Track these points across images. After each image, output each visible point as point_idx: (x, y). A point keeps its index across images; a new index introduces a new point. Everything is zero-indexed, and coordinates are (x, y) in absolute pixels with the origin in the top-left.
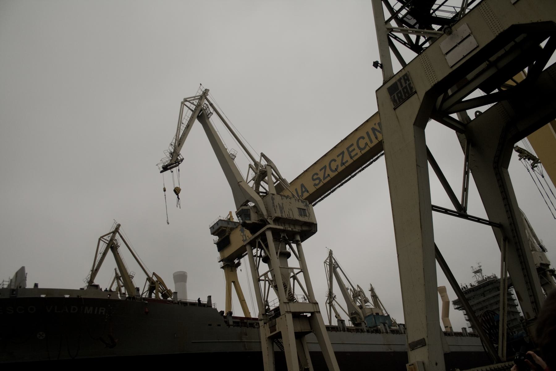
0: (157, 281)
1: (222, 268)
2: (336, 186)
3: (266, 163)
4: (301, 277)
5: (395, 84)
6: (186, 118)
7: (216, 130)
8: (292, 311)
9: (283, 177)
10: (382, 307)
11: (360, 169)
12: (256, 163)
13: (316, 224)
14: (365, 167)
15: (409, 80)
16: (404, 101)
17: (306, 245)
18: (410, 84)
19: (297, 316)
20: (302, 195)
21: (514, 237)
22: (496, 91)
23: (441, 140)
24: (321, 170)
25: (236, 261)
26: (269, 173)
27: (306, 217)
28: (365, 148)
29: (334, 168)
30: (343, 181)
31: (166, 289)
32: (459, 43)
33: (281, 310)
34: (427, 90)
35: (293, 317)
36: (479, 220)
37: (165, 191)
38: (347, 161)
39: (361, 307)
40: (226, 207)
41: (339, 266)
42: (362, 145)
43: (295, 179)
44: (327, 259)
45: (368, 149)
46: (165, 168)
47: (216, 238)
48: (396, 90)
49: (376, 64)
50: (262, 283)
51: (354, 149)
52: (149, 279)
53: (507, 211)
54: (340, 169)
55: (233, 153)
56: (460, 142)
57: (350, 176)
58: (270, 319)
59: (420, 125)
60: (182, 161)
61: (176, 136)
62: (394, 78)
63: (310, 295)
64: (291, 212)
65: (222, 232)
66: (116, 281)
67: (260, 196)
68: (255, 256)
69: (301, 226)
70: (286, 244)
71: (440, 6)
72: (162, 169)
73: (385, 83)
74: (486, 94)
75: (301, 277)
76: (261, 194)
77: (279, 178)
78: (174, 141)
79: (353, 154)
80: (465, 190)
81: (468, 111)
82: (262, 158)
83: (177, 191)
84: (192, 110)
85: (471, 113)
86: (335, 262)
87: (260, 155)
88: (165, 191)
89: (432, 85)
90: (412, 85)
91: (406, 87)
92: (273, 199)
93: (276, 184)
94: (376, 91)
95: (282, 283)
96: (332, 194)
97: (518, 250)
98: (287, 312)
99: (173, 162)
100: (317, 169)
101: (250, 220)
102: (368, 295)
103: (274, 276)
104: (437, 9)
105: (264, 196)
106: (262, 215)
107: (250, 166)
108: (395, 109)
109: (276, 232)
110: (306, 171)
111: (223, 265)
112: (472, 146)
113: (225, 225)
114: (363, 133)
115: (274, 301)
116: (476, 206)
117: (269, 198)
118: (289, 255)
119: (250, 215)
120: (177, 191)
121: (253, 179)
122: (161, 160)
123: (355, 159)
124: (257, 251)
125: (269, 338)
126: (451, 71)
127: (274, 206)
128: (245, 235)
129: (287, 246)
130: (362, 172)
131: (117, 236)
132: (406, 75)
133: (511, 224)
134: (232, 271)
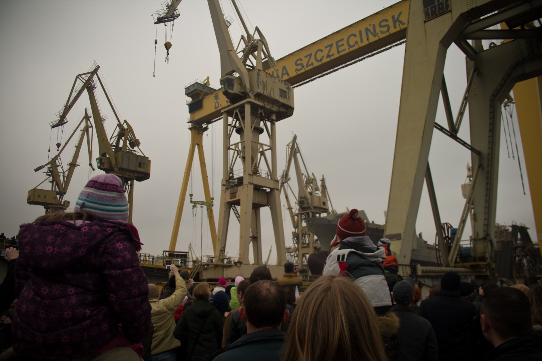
0: (127, 129)
1: (190, 129)
2: (317, 76)
3: (259, 38)
4: (268, 154)
8: (255, 183)
9: (272, 55)
10: (328, 198)
11: (344, 65)
12: (249, 35)
13: (293, 108)
14: (349, 65)
16: (437, 16)
17: (279, 124)
19: (258, 189)
20: (282, 77)
21: (488, 166)
22: (519, 28)
23: (456, 62)
24: (306, 57)
25: (204, 126)
26: (259, 49)
27: (285, 100)
28: (354, 46)
29: (319, 58)
30: (324, 73)
36: (464, 144)
37: (156, 43)
38: (333, 55)
39: (311, 194)
41: (299, 152)
42: (352, 42)
44: (290, 143)
45: (356, 47)
46: (160, 20)
47: (190, 100)
50: (231, 152)
51: (343, 45)
52: (120, 125)
54: (325, 60)
55: (229, 20)
56: (467, 68)
57: (332, 70)
58: (232, 187)
59: (445, 44)
60: (178, 17)
63: (272, 173)
64: (272, 91)
65: (197, 94)
66: (84, 121)
67: (247, 69)
68: (230, 125)
69: (279, 107)
72: (156, 21)
75: (268, 154)
76: (247, 67)
77: (269, 56)
80: (461, 114)
82: (256, 32)
83: (168, 46)
85: (486, 44)
86: (298, 147)
87: (255, 29)
88: (156, 43)
89: (470, 8)
90: (449, 3)
91: (442, 3)
92: (258, 75)
95: (251, 155)
96: (311, 83)
98: (250, 183)
99: (169, 16)
100: (302, 55)
101: (232, 90)
103: (244, 148)
107: (242, 37)
108: (425, 22)
109: (254, 108)
110: (291, 54)
111: (191, 127)
113: (201, 88)
115: (239, 170)
117: (255, 73)
118: (261, 131)
119: (233, 85)
120: (168, 46)
121: (243, 51)
122: (157, 11)
123: (342, 54)
124: (233, 120)
127: (258, 81)
128: (218, 103)
129: (262, 123)
131: (95, 78)
133: (489, 154)
134: (198, 134)
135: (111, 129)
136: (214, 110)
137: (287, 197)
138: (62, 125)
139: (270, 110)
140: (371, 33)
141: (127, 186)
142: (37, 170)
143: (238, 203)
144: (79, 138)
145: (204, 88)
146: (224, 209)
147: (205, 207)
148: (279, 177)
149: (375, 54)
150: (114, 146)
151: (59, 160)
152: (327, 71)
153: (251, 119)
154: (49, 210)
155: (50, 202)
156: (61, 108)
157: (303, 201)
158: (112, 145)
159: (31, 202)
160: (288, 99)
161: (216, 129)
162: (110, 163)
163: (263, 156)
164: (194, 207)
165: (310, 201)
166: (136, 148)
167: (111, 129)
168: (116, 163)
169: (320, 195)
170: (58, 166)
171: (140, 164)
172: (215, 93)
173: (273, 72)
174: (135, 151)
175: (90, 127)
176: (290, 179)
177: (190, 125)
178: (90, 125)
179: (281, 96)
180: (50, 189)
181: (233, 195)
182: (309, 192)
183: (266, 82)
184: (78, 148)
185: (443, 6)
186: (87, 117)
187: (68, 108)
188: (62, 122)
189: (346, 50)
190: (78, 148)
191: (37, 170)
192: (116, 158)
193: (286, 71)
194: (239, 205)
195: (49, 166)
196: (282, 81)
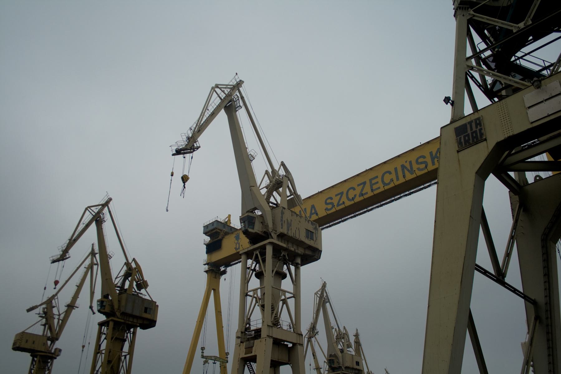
0: (135, 269)
1: (206, 272)
2: (349, 217)
3: (285, 174)
5: (465, 126)
6: (213, 105)
7: (241, 126)
8: (275, 336)
9: (299, 192)
10: (363, 357)
14: (384, 204)
15: (481, 126)
16: (471, 145)
17: (305, 269)
18: (480, 130)
19: (277, 343)
20: (310, 217)
23: (496, 197)
24: (336, 195)
25: (222, 269)
26: (284, 185)
28: (389, 184)
30: (357, 213)
31: (143, 279)
32: (546, 100)
33: (262, 333)
34: (499, 140)
35: (273, 343)
36: (515, 291)
37: (172, 175)
38: (367, 193)
39: (342, 351)
40: (229, 208)
42: (387, 180)
43: (307, 198)
44: (319, 291)
45: (392, 185)
46: (178, 152)
47: (208, 239)
48: (465, 132)
49: (447, 100)
50: (249, 299)
51: (377, 183)
52: (127, 264)
53: (546, 289)
54: (358, 199)
55: (252, 154)
56: (511, 204)
57: (366, 210)
58: (248, 340)
59: (482, 175)
60: (198, 149)
61: (198, 121)
62: (464, 119)
63: (295, 325)
64: (297, 231)
65: (216, 234)
66: (90, 257)
67: (270, 206)
68: (249, 268)
69: (305, 249)
70: (285, 264)
71: (526, 55)
72: (175, 152)
73: (452, 122)
74: (553, 160)
76: (271, 205)
78: (195, 126)
79: (375, 187)
80: (508, 255)
81: (527, 173)
82: (282, 167)
83: (185, 179)
84: (221, 98)
85: (530, 176)
86: (327, 296)
88: (172, 175)
89: (506, 136)
91: (476, 132)
92: (283, 213)
93: (290, 198)
94: (442, 128)
95: (271, 303)
96: (342, 223)
97: (548, 333)
99: (189, 147)
101: (253, 229)
102: (352, 339)
103: (263, 294)
104: (522, 57)
105: (273, 208)
106: (267, 226)
107: (267, 173)
108: (458, 152)
109: (277, 250)
110: (321, 192)
111: (207, 269)
112: (523, 211)
113: (220, 227)
114: (391, 168)
115: (257, 320)
116: (514, 276)
117: (278, 211)
118: (284, 276)
119: (254, 223)
120: (185, 179)
121: (266, 187)
122: (176, 143)
123: (376, 192)
124: (253, 263)
125: (242, 359)
126: (530, 126)
127: (282, 220)
129: (285, 266)
130: (380, 208)
131: (106, 210)
132: (478, 119)
133: (546, 304)
134: (215, 278)
135: (117, 268)
136: (234, 251)
137: (314, 355)
138: (63, 260)
139: (294, 252)
140: (408, 170)
141: (129, 334)
142: (28, 310)
143: (253, 359)
144: (81, 278)
145: (224, 227)
146: (237, 366)
147: (218, 363)
148: (304, 329)
149: (412, 193)
150: (118, 287)
151: (56, 300)
152: (360, 211)
153: (273, 261)
154: (36, 359)
155: (39, 349)
156: (65, 241)
157: (333, 360)
158: (116, 286)
159: (16, 348)
160: (316, 241)
161: (234, 272)
162: (112, 306)
163: (285, 305)
164: (205, 362)
165: (341, 360)
166: (143, 291)
167: (117, 268)
168: (119, 306)
169: (354, 353)
170: (54, 307)
171: (146, 309)
172: (236, 233)
173: (300, 211)
174: (141, 294)
175: (96, 264)
176: (317, 332)
177: (206, 267)
178: (95, 262)
179: (307, 237)
180: (41, 333)
181: (249, 349)
182: (340, 349)
183: (291, 221)
184: (80, 287)
185: (477, 135)
186: (93, 254)
187: (72, 242)
188: (63, 257)
189: (380, 188)
190: (80, 287)
191: (28, 310)
192: (119, 301)
193: (315, 210)
194: (255, 362)
195: (44, 306)
196: (308, 221)
